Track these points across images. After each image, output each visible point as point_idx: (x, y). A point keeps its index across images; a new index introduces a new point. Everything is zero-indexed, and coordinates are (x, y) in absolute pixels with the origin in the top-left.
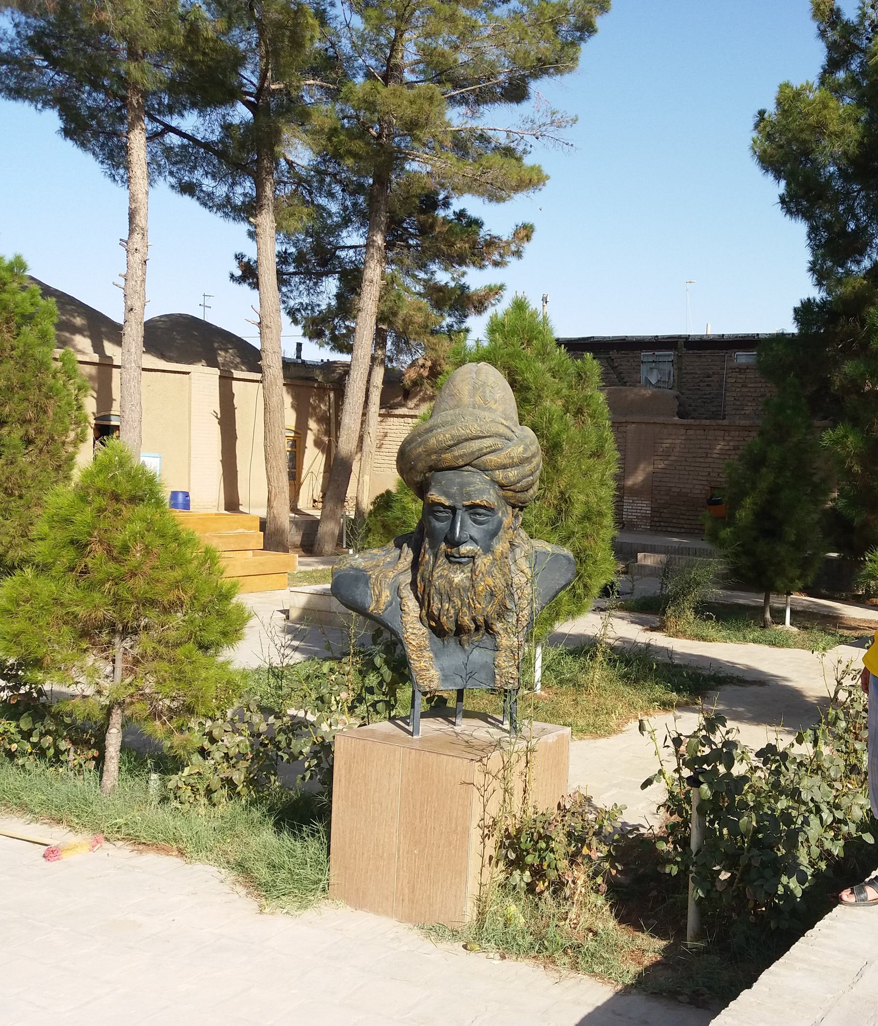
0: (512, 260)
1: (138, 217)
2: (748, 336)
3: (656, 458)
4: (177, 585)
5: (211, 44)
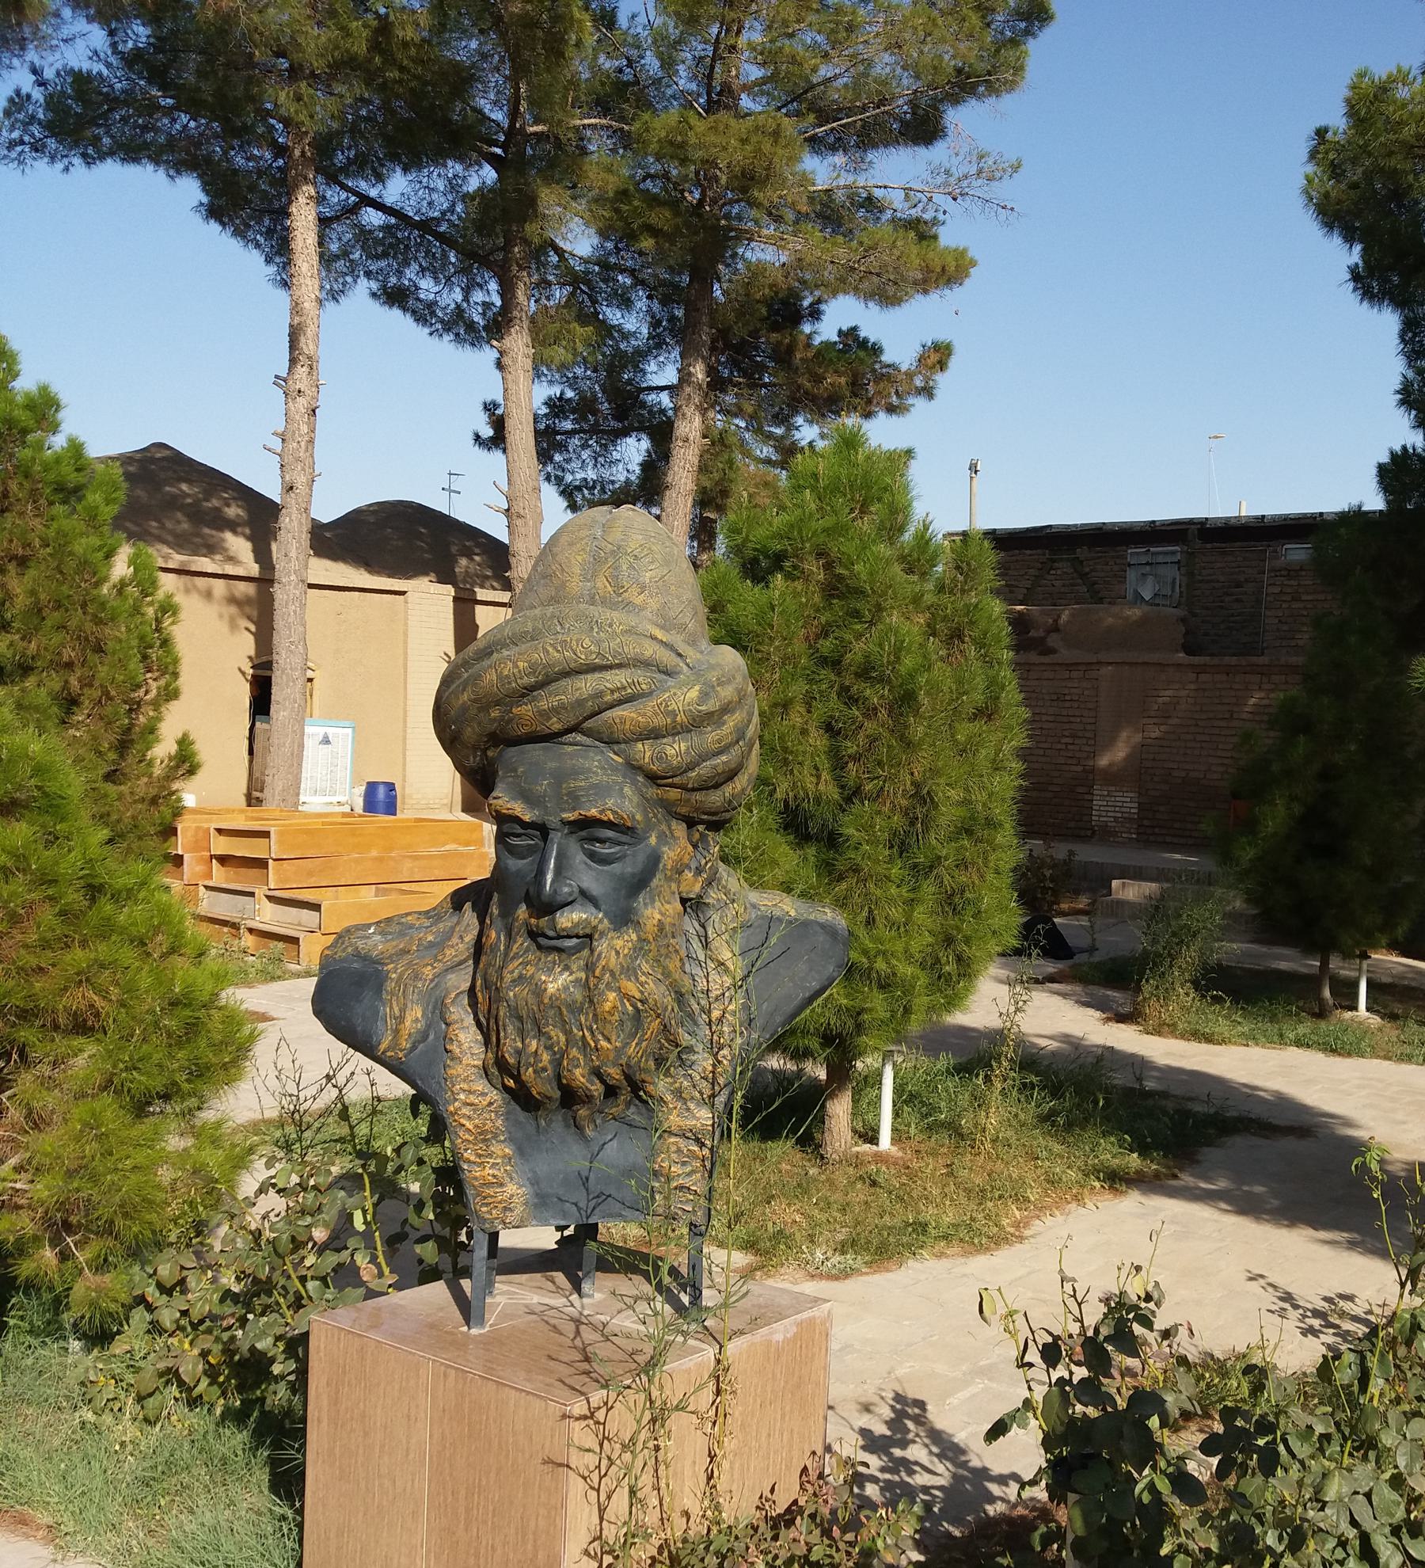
0: (918, 403)
1: (302, 339)
2: (1304, 517)
3: (1145, 721)
4: (83, 978)
5: (413, 51)
